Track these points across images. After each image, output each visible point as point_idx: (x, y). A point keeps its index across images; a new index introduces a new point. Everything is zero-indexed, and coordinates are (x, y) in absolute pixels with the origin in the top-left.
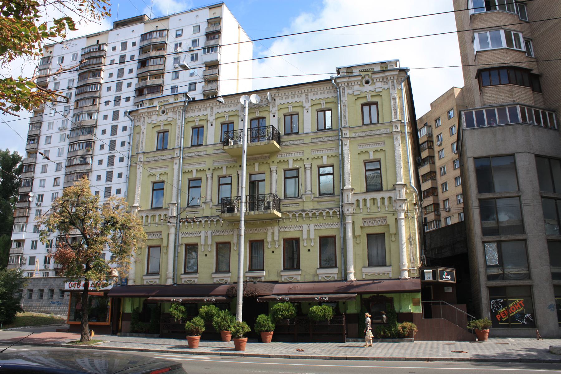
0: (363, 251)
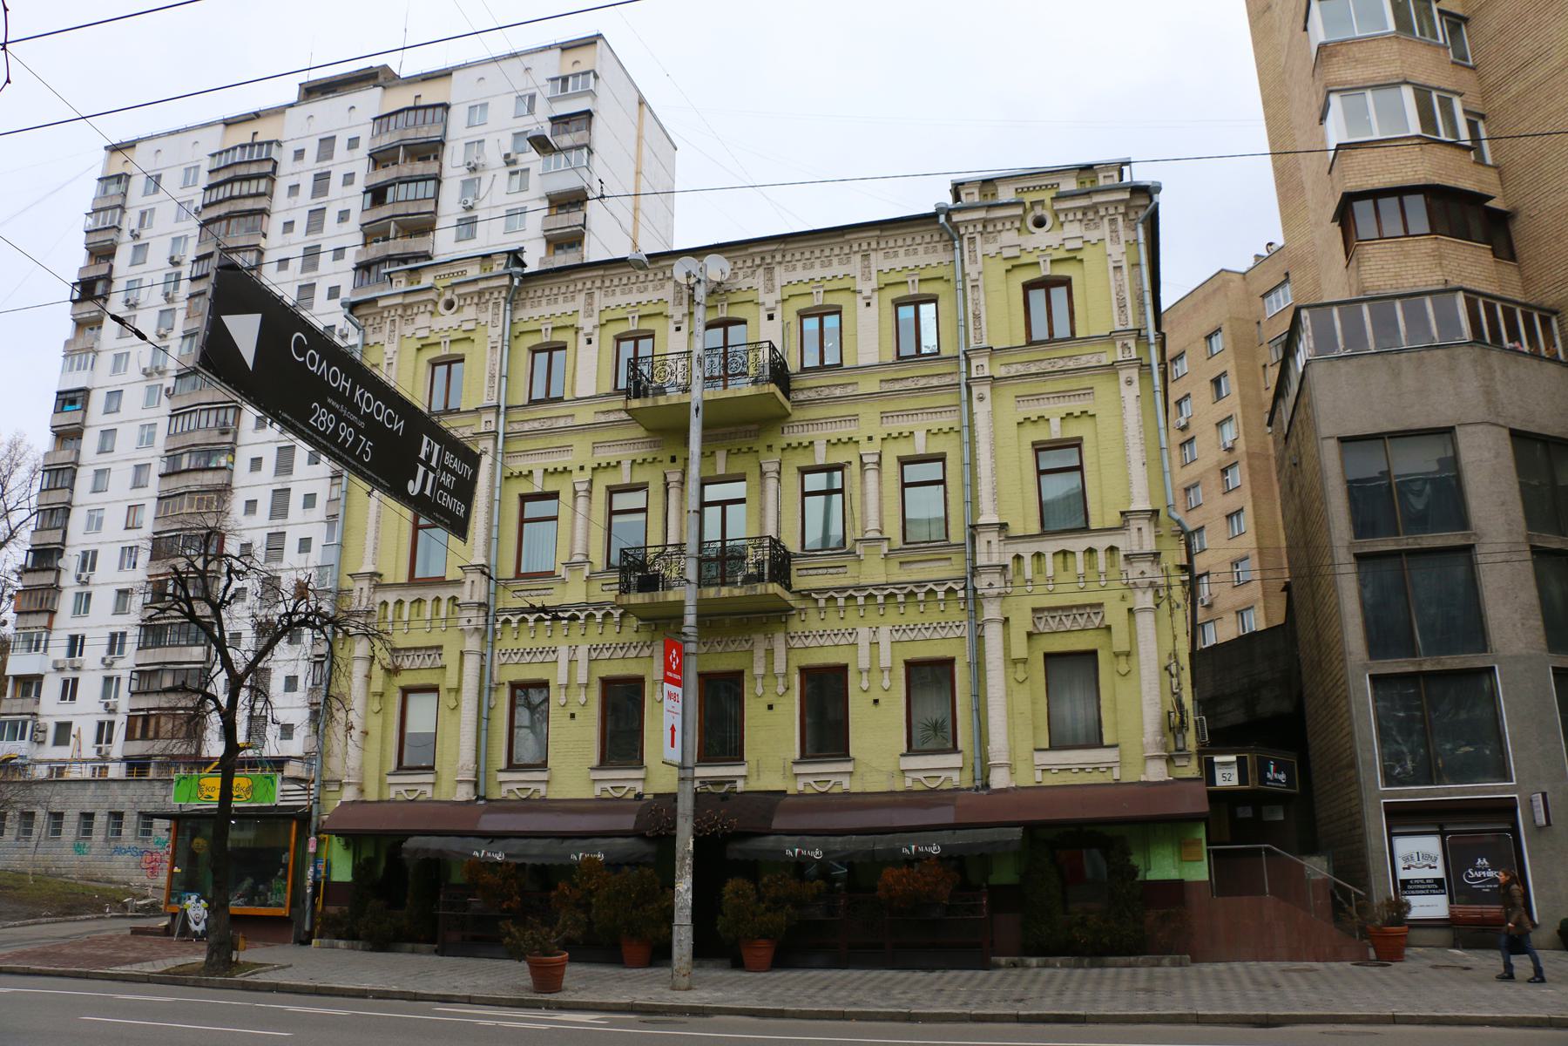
0: (1034, 703)
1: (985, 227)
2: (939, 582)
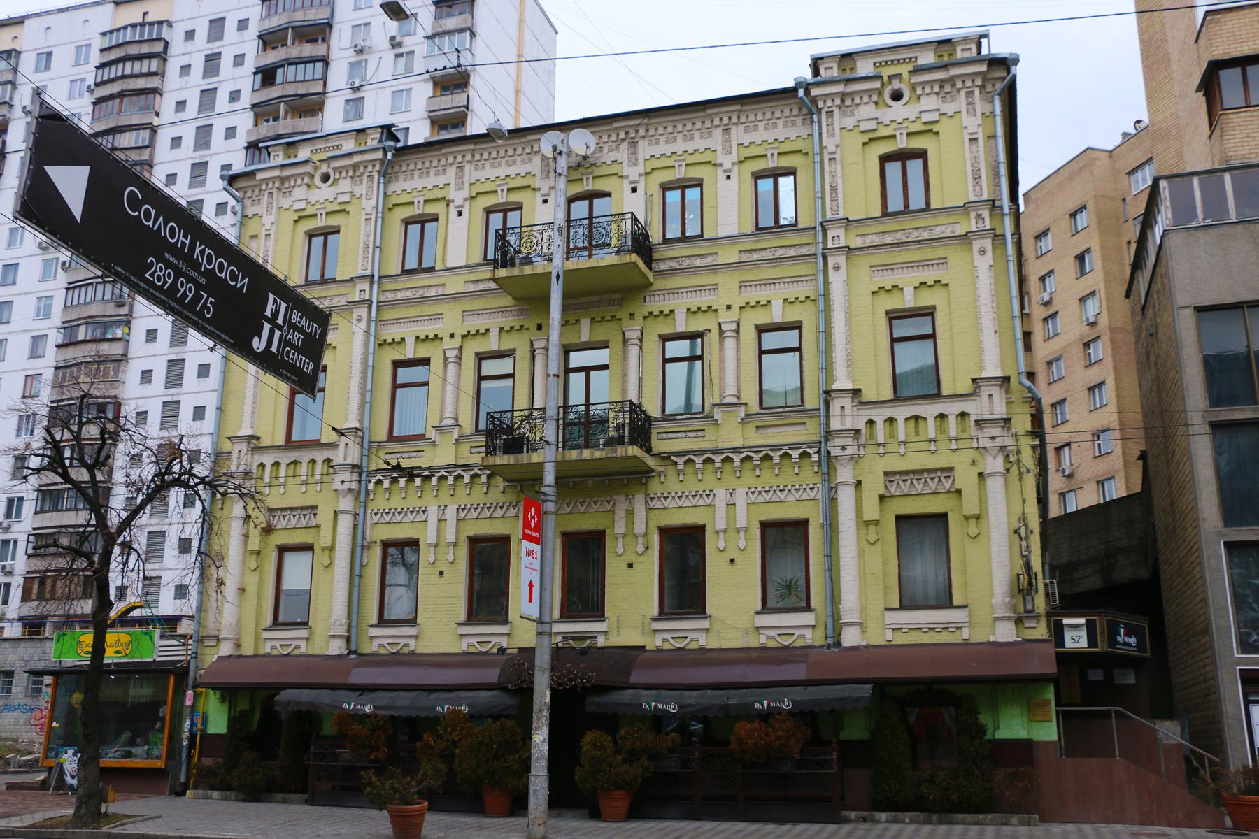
0: (885, 563)
1: (843, 101)
2: (794, 446)
